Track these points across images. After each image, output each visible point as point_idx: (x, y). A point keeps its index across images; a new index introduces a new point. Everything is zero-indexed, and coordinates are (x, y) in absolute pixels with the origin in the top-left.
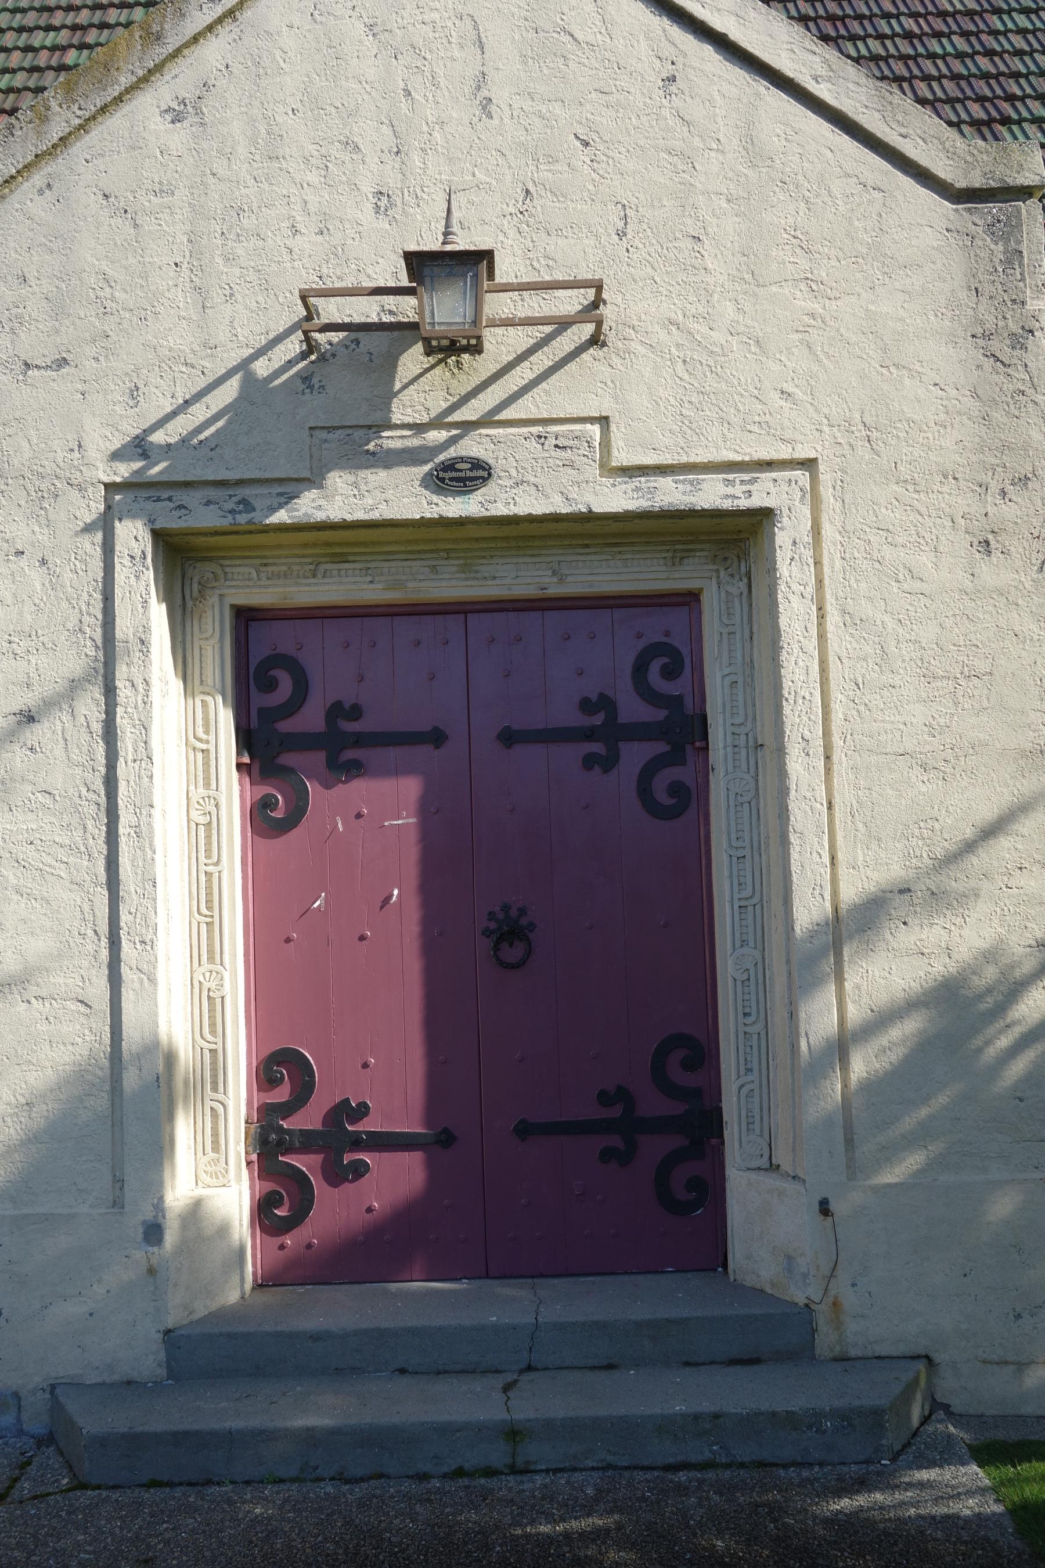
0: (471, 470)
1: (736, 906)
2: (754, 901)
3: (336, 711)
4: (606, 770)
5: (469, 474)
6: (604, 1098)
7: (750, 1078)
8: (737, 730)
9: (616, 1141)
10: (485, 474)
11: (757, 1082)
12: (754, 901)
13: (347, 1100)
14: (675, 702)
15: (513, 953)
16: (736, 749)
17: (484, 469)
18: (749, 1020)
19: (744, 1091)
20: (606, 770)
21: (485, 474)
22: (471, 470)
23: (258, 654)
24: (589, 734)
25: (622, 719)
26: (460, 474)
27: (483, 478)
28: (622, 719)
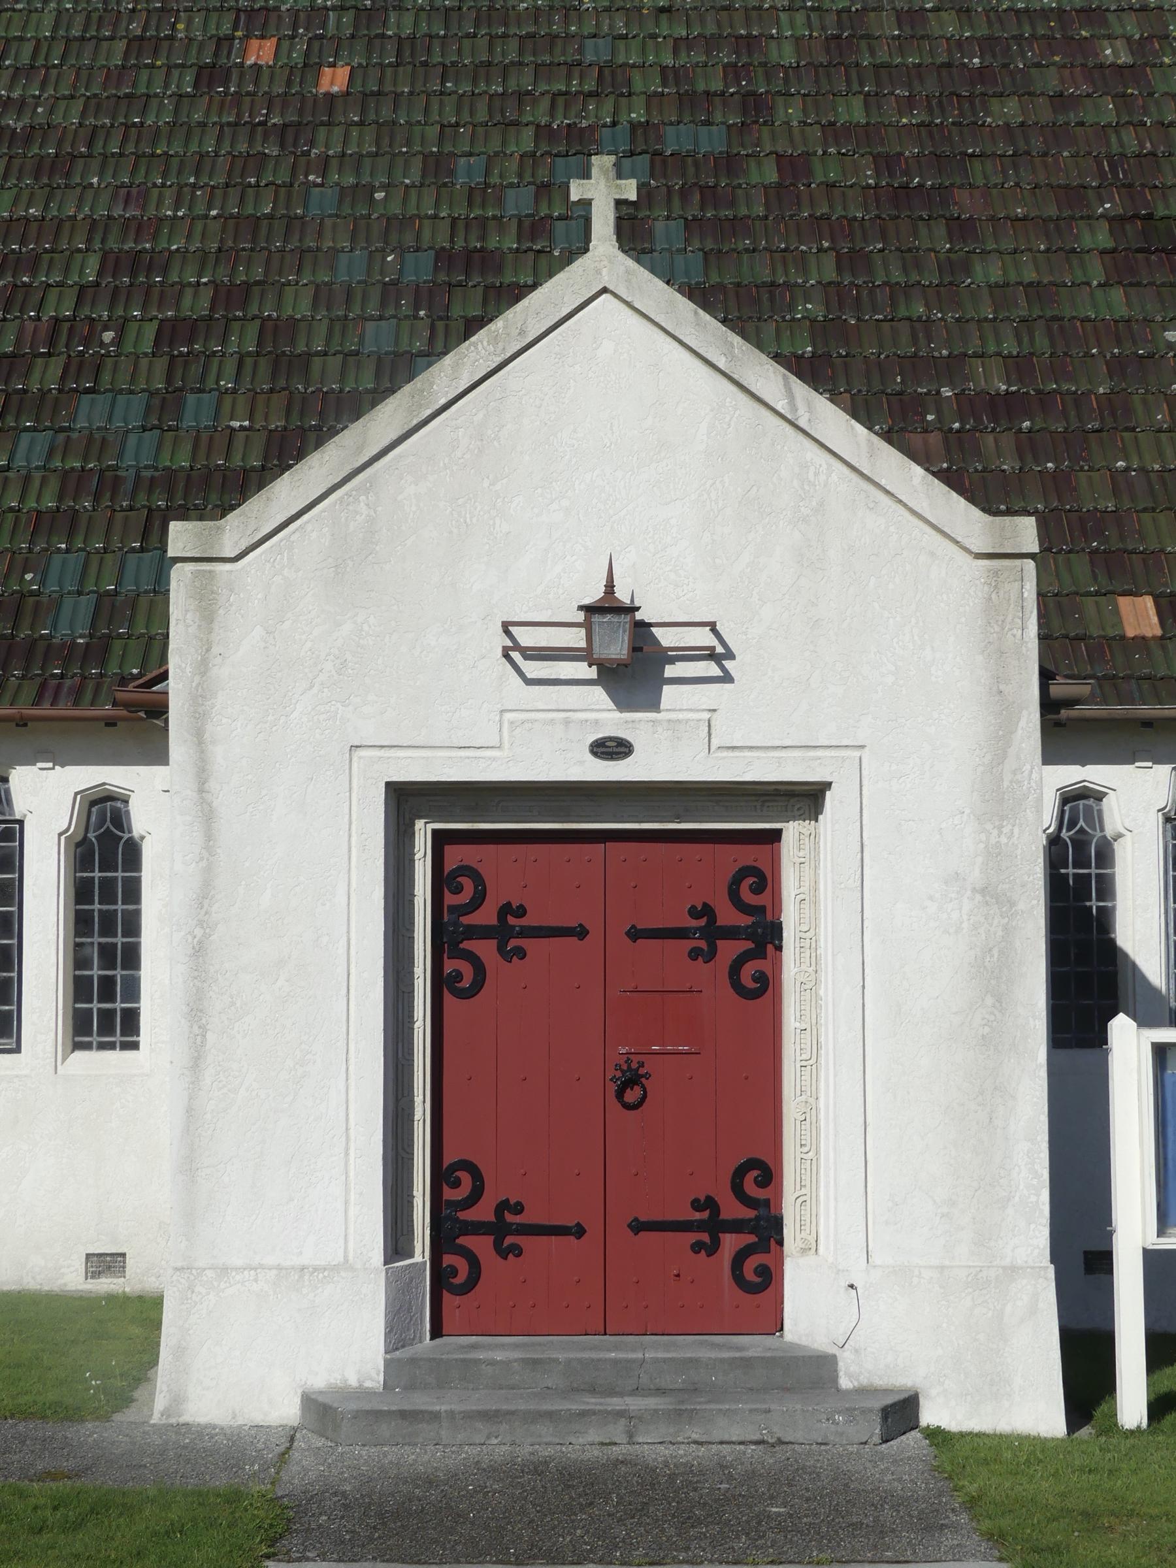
0: (617, 747)
1: (798, 1066)
2: (811, 1062)
3: (506, 910)
4: (509, 904)
5: (615, 750)
6: (696, 1205)
7: (804, 1191)
8: (803, 935)
9: (705, 1237)
10: (627, 750)
11: (809, 1195)
12: (811, 1062)
13: (507, 1200)
14: (762, 910)
15: (631, 1096)
16: (802, 950)
17: (626, 747)
18: (805, 1149)
19: (800, 1201)
20: (509, 904)
21: (627, 750)
22: (617, 747)
23: (450, 865)
24: (698, 1226)
25: (490, 1240)
26: (611, 750)
27: (625, 753)
28: (490, 1240)
